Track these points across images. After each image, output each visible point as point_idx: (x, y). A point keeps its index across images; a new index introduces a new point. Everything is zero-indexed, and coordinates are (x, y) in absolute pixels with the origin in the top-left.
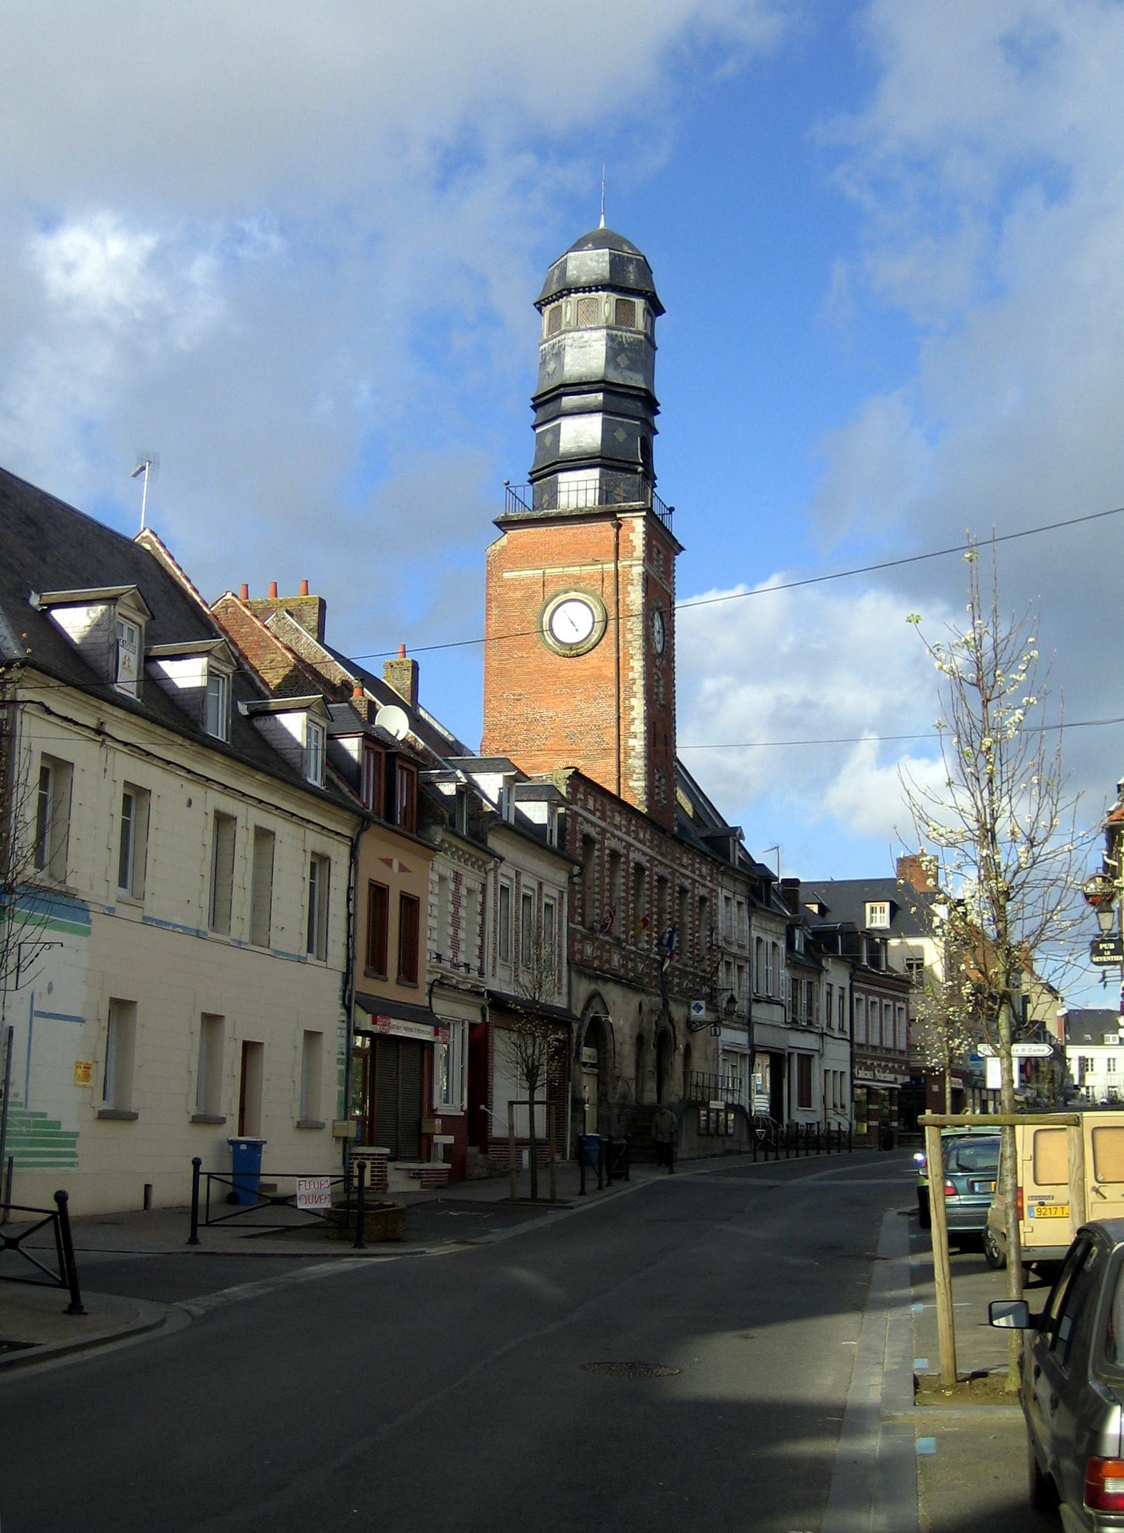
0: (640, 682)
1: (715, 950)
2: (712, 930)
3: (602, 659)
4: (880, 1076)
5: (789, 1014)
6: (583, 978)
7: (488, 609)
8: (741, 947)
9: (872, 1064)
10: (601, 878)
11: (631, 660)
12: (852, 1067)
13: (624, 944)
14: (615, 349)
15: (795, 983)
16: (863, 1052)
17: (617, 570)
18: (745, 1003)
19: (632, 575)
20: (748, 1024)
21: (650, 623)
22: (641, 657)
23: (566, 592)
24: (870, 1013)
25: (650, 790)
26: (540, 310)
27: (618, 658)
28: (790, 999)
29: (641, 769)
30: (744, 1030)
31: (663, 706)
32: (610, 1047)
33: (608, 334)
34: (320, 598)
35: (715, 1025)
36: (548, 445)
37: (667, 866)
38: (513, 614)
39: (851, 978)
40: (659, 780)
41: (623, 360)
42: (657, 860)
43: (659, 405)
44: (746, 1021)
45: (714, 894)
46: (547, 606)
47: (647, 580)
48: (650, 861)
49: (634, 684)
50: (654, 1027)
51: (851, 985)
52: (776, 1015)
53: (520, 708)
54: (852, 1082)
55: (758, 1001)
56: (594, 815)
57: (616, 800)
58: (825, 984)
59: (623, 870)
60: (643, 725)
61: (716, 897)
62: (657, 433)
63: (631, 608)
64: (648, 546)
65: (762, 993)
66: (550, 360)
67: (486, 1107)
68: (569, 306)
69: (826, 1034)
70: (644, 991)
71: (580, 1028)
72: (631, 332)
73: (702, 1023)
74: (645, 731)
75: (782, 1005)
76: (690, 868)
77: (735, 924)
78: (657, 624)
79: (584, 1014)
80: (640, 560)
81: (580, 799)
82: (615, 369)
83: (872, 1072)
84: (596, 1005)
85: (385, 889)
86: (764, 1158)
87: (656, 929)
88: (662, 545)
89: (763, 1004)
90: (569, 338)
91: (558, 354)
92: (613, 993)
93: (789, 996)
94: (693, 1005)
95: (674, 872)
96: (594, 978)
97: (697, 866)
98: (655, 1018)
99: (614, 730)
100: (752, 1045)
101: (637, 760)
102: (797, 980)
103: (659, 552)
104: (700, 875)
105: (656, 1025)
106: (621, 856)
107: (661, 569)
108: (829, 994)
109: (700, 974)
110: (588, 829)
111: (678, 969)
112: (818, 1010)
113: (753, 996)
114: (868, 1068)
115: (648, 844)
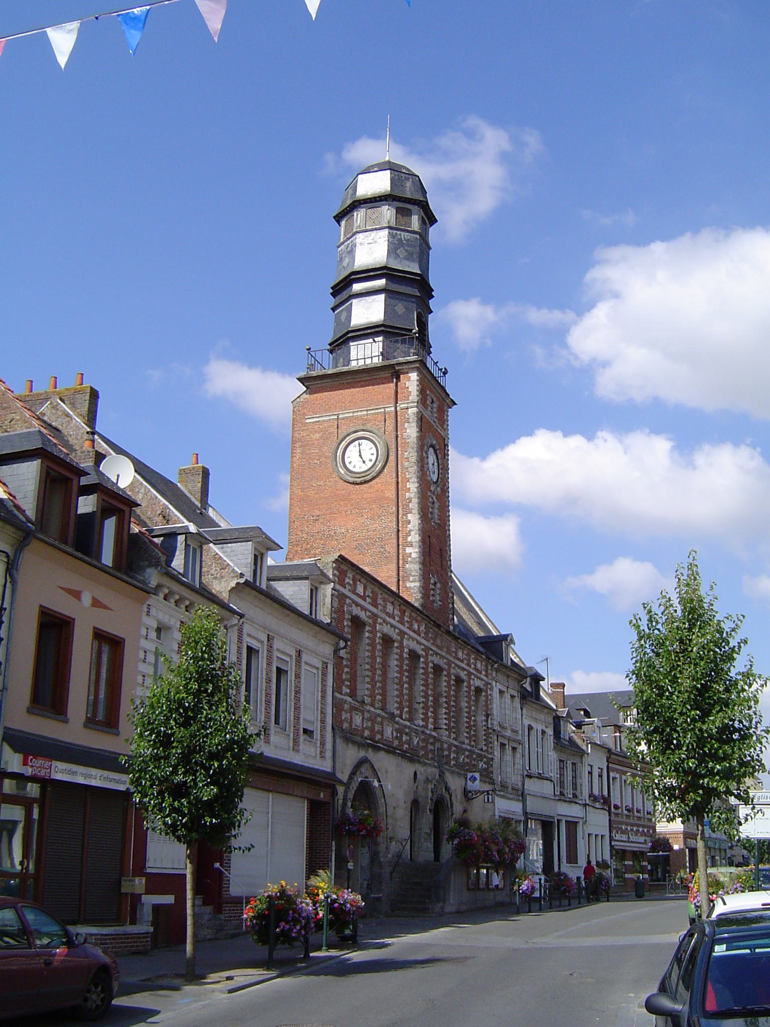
0: (415, 501)
1: (491, 733)
2: (487, 716)
3: (385, 485)
4: (633, 838)
5: (558, 789)
6: (350, 744)
7: (293, 448)
8: (515, 731)
9: (627, 829)
10: (373, 657)
11: (408, 483)
12: (610, 832)
13: (397, 719)
14: (395, 244)
15: (562, 764)
16: (620, 819)
17: (396, 412)
18: (519, 778)
19: (408, 415)
20: (521, 795)
21: (424, 454)
22: (416, 480)
23: (356, 432)
24: (623, 789)
25: (426, 590)
26: (339, 222)
27: (398, 483)
28: (559, 776)
29: (417, 572)
30: (519, 800)
31: (439, 525)
32: (382, 809)
33: (389, 233)
34: (92, 388)
35: (488, 794)
36: (343, 320)
37: (442, 657)
38: (313, 451)
39: (607, 761)
40: (435, 584)
41: (401, 252)
42: (431, 649)
43: (433, 291)
44: (520, 793)
45: (489, 686)
46: (340, 444)
47: (421, 420)
48: (427, 649)
49: (410, 502)
50: (430, 794)
51: (608, 766)
52: (547, 788)
53: (318, 527)
54: (611, 843)
55: (530, 776)
56: (365, 600)
57: (396, 595)
58: (586, 764)
59: (396, 654)
60: (417, 535)
61: (491, 689)
62: (431, 312)
63: (407, 441)
64: (422, 392)
65: (534, 770)
66: (345, 257)
67: (221, 865)
68: (359, 215)
69: (588, 805)
70: (419, 762)
71: (346, 792)
72: (408, 231)
73: (477, 792)
74: (419, 540)
75: (552, 781)
76: (465, 662)
77: (508, 712)
78: (432, 458)
79: (351, 778)
80: (414, 402)
81: (349, 583)
82: (396, 259)
83: (627, 836)
84: (365, 770)
85: (120, 642)
86: (527, 910)
87: (431, 709)
88: (436, 397)
89: (536, 780)
90: (360, 237)
91: (351, 252)
92: (383, 761)
93: (557, 774)
94: (468, 778)
95: (449, 663)
96: (361, 745)
97: (472, 661)
98: (430, 786)
99: (395, 541)
100: (525, 813)
101: (413, 564)
102: (563, 761)
103: (433, 402)
104: (477, 670)
105: (432, 792)
106: (394, 641)
107: (435, 415)
108: (590, 773)
109: (477, 751)
110: (356, 611)
111: (456, 746)
112: (581, 785)
113: (525, 773)
114: (624, 832)
115: (423, 635)
